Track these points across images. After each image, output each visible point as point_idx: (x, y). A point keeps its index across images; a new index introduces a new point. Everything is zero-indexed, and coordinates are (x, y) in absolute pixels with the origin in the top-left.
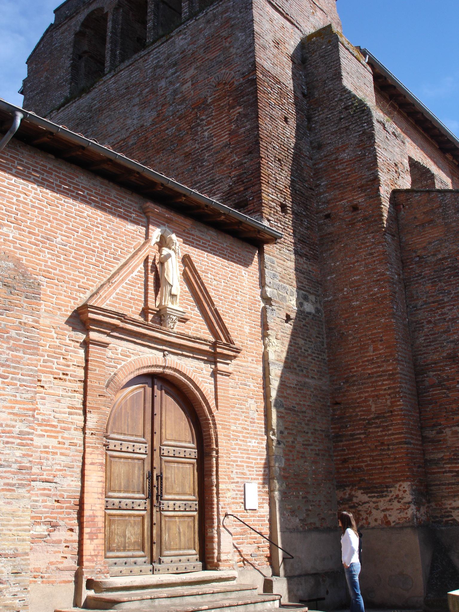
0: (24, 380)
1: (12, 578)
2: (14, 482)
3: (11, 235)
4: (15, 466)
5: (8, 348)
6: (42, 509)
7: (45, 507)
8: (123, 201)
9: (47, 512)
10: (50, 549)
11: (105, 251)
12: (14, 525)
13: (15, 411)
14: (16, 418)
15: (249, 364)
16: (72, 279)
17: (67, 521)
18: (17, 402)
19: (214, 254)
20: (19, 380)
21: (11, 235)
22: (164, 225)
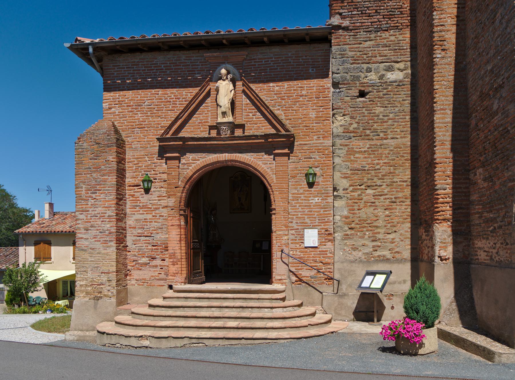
0: (109, 190)
1: (108, 284)
2: (107, 239)
3: (117, 111)
4: (107, 232)
5: (100, 175)
6: (145, 250)
7: (147, 249)
8: (191, 60)
9: (149, 252)
10: (151, 269)
11: (179, 99)
12: (108, 259)
13: (106, 206)
14: (106, 209)
15: (315, 141)
16: (156, 124)
17: (161, 256)
18: (106, 201)
19: (119, 91)
20: (107, 190)
21: (117, 111)
22: (224, 63)
